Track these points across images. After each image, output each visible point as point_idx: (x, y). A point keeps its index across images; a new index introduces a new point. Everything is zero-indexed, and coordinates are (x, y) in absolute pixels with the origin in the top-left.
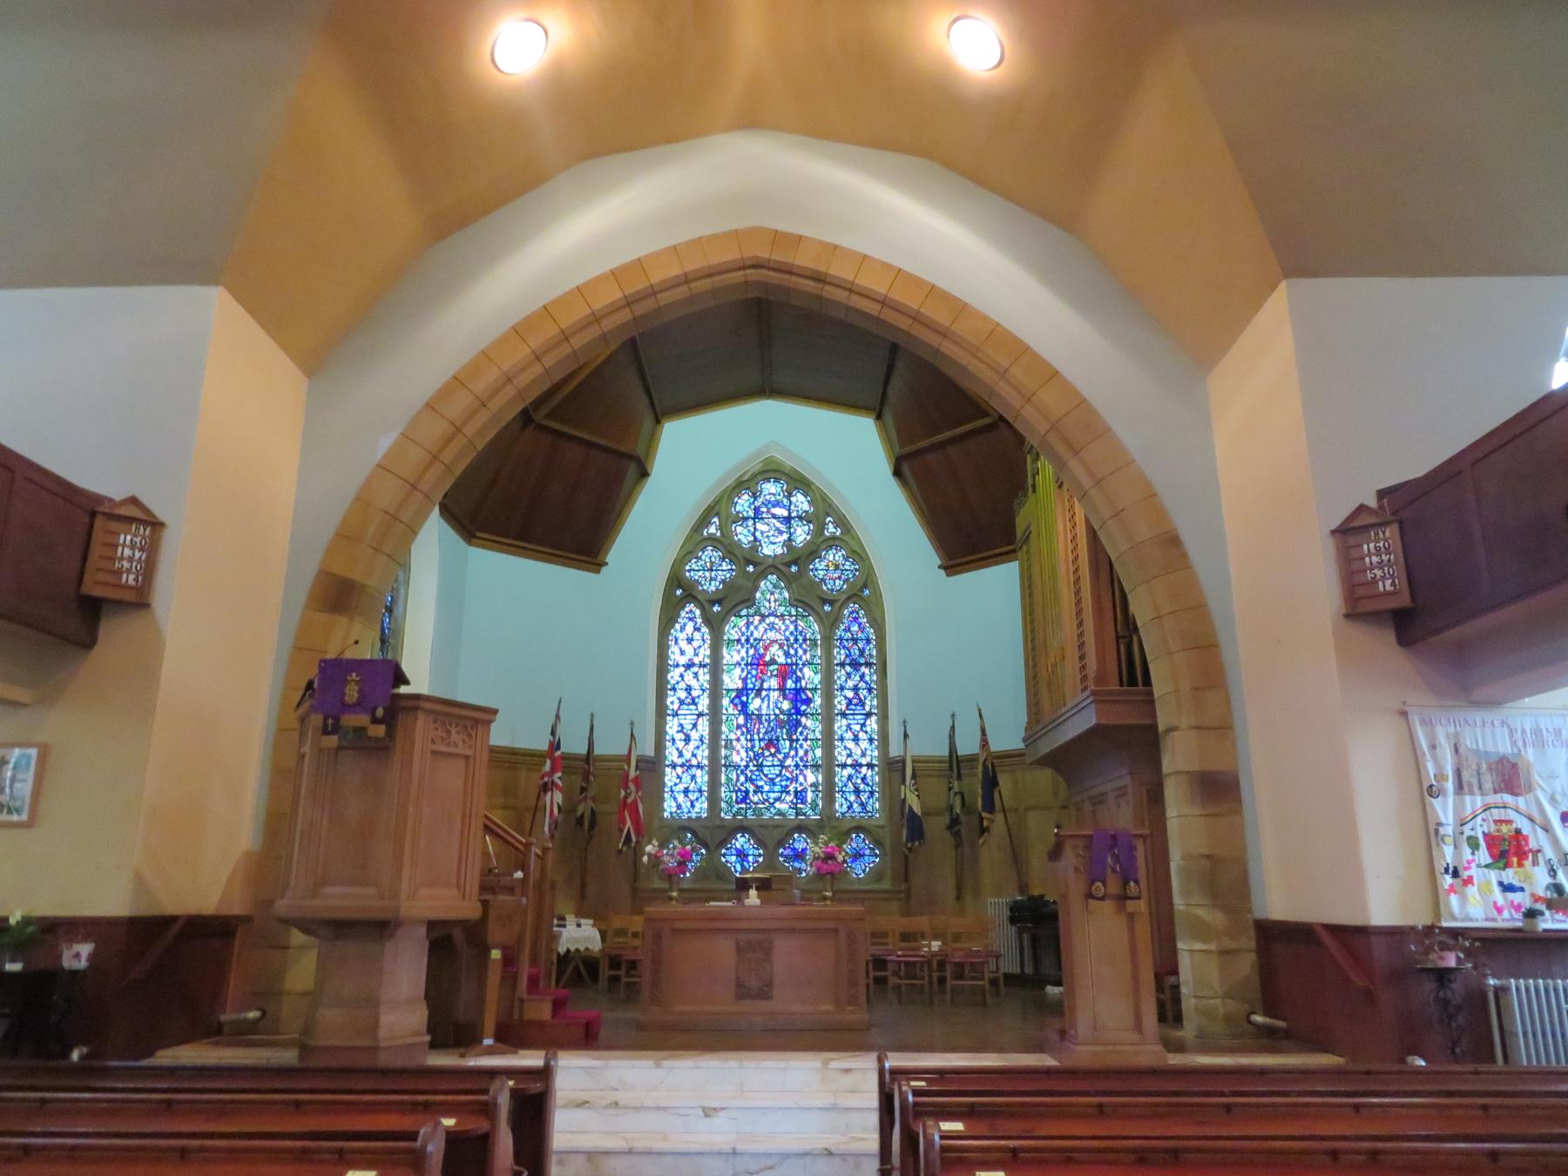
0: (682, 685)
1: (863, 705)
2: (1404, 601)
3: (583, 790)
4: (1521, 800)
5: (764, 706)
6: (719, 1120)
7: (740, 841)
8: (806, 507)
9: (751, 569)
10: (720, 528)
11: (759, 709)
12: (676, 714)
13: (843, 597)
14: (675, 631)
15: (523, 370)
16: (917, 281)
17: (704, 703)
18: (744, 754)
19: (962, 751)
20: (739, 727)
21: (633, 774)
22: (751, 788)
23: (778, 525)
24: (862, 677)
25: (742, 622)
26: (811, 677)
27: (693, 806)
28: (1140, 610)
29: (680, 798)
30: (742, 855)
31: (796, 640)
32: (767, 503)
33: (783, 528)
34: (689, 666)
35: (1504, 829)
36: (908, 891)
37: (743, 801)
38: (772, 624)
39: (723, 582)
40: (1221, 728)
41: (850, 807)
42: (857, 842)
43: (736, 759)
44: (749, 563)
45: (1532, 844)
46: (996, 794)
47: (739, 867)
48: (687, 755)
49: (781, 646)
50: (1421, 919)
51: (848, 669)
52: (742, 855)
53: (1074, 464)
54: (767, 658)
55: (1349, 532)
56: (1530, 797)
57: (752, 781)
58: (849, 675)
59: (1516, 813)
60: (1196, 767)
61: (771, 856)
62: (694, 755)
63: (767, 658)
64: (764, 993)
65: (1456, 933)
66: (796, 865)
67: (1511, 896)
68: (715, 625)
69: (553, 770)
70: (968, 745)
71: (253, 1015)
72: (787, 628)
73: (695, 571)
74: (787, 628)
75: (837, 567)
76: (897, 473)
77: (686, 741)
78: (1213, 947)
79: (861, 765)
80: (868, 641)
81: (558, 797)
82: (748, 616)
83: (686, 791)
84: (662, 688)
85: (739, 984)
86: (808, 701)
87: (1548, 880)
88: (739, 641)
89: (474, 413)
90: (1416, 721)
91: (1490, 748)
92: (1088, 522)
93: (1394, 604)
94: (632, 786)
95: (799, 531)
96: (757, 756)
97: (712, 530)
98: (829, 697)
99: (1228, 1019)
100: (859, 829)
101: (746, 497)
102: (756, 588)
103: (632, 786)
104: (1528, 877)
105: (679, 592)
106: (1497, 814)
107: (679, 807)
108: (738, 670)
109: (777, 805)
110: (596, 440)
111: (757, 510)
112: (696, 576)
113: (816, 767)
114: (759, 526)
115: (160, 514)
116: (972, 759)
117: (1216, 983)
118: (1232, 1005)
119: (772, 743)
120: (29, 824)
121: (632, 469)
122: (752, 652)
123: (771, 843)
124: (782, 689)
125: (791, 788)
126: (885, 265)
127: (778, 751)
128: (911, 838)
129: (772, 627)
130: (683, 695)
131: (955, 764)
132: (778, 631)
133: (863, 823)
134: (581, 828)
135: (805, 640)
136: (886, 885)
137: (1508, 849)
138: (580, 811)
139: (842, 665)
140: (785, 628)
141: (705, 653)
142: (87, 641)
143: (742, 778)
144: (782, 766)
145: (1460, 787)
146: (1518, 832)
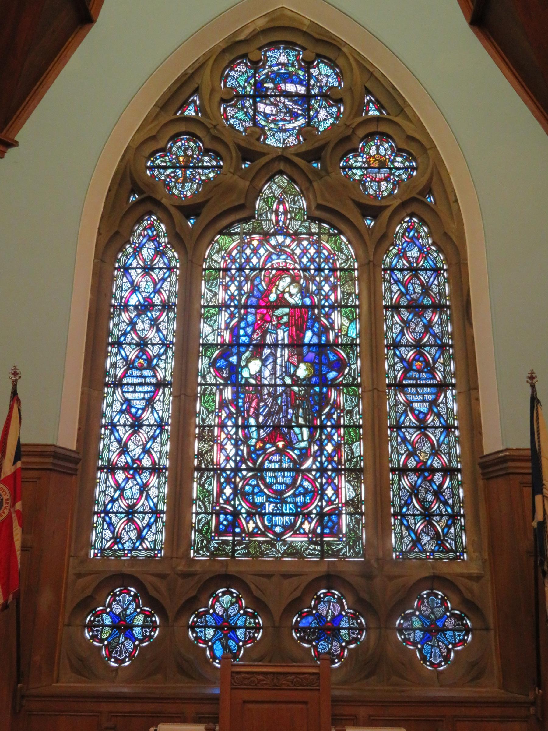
0: (132, 337)
1: (432, 371)
5: (267, 373)
7: (224, 602)
8: (333, 81)
10: (200, 109)
11: (258, 376)
12: (118, 384)
13: (396, 203)
14: (126, 256)
17: (166, 369)
18: (230, 448)
20: (223, 404)
22: (244, 508)
23: (289, 104)
24: (428, 327)
25: (231, 243)
26: (345, 326)
27: (141, 538)
29: (119, 522)
30: (226, 627)
32: (273, 77)
33: (298, 109)
34: (145, 307)
37: (230, 529)
38: (283, 250)
39: (203, 183)
41: (417, 541)
42: (429, 605)
43: (219, 457)
44: (251, 157)
47: (219, 651)
48: (135, 451)
49: (295, 280)
51: (405, 314)
52: (226, 627)
54: (273, 297)
57: (245, 495)
58: (406, 324)
61: (277, 629)
62: (147, 451)
63: (273, 297)
66: (323, 646)
68: (189, 246)
72: (305, 251)
74: (305, 251)
77: (134, 435)
79: (433, 471)
84: (98, 341)
88: (227, 270)
95: (323, 114)
97: (190, 112)
98: (375, 360)
100: (436, 580)
101: (242, 68)
107: (117, 539)
108: (224, 316)
109: (289, 538)
110: (303, 664)
111: (258, 85)
112: (162, 176)
113: (354, 473)
114: (261, 107)
119: (278, 432)
122: (246, 288)
123: (277, 609)
124: (296, 344)
125: (313, 508)
127: (290, 445)
129: (280, 249)
130: (131, 353)
132: (291, 255)
133: (445, 570)
135: (333, 270)
136: (490, 689)
139: (395, 308)
140: (303, 252)
141: (170, 288)
143: (228, 491)
144: (297, 470)
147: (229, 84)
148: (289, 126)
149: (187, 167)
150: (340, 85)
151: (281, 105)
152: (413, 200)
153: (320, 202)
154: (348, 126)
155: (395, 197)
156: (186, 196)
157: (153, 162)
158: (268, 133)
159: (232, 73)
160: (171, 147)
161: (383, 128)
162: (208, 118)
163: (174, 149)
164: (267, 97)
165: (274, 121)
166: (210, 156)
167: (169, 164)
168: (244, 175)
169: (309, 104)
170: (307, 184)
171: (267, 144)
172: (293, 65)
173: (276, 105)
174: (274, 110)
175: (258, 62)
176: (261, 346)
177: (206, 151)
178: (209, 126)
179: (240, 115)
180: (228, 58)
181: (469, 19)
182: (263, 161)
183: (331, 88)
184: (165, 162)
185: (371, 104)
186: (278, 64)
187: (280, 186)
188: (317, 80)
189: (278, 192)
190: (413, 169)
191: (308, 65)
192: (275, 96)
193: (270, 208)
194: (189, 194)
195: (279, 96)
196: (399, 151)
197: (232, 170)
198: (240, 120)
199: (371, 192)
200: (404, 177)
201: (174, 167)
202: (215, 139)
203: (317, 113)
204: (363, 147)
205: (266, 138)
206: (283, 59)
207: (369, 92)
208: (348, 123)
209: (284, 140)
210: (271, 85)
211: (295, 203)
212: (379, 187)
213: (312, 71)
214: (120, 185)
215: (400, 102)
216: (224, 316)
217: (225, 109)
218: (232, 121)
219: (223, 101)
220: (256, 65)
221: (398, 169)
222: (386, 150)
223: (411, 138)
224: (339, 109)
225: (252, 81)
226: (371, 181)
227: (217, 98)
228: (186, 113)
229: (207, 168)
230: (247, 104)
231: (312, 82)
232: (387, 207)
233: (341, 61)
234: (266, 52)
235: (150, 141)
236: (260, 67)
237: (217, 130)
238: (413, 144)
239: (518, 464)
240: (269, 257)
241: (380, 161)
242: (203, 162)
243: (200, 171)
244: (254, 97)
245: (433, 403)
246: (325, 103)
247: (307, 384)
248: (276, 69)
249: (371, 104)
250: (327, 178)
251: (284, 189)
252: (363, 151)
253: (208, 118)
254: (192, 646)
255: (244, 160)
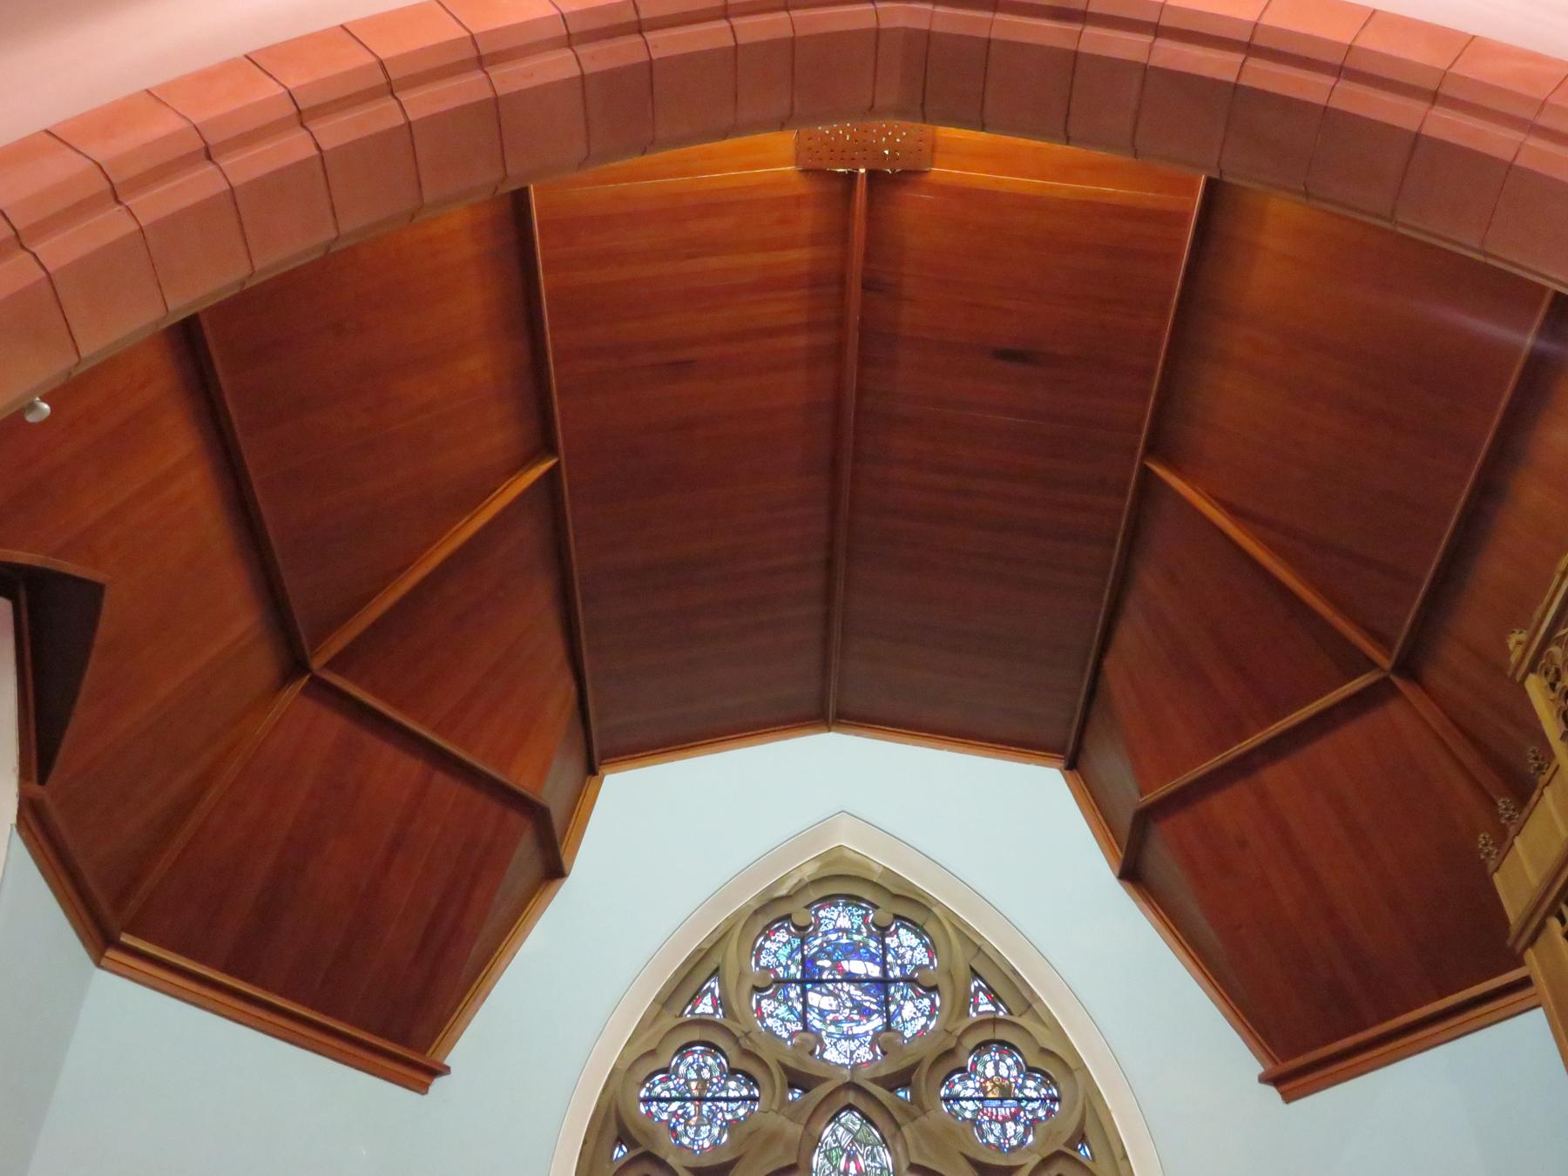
8: (921, 956)
10: (721, 1002)
13: (1033, 1161)
15: (246, 139)
33: (870, 1002)
39: (730, 1126)
76: (1131, 873)
89: (80, 209)
95: (909, 1010)
97: (705, 1007)
101: (782, 936)
105: (619, 1153)
112: (663, 1113)
114: (814, 998)
121: (525, 851)
147: (763, 962)
148: (857, 1030)
149: (702, 1099)
150: (931, 962)
151: (844, 996)
152: (1058, 1155)
153: (916, 1160)
154: (949, 1033)
155: (1030, 1149)
156: (702, 1149)
157: (649, 1090)
158: (827, 1041)
159: (768, 944)
160: (677, 1065)
161: (1003, 1034)
162: (736, 1020)
163: (682, 1069)
164: (821, 982)
165: (835, 1022)
166: (738, 1080)
167: (674, 1093)
168: (793, 1111)
169: (887, 993)
170: (893, 1129)
171: (825, 1061)
172: (859, 932)
173: (837, 997)
174: (835, 1003)
175: (806, 928)
177: (733, 1072)
178: (738, 1034)
179: (782, 1011)
180: (764, 921)
181: (1117, 870)
182: (820, 1092)
183: (919, 968)
184: (669, 1090)
185: (981, 994)
186: (836, 930)
187: (849, 1130)
188: (897, 956)
189: (846, 1140)
190: (1054, 1100)
191: (882, 932)
192: (834, 981)
193: (835, 1168)
194: (707, 1144)
195: (841, 981)
196: (1030, 1071)
197: (775, 1107)
198: (783, 1020)
199: (992, 1139)
200: (1041, 1113)
201: (683, 1099)
202: (748, 1060)
203: (901, 1007)
204: (974, 1063)
205: (823, 1050)
206: (844, 922)
207: (976, 975)
208: (950, 1028)
209: (852, 1053)
210: (826, 963)
211: (874, 1160)
212: (1004, 1130)
213: (888, 940)
214: (601, 1133)
215: (1026, 994)
217: (758, 1002)
218: (770, 1022)
219: (757, 989)
220: (803, 932)
221: (1030, 1100)
222: (1009, 1068)
223: (1045, 1051)
224: (933, 1001)
225: (799, 957)
226: (990, 1121)
227: (747, 987)
228: (698, 1011)
229: (735, 1100)
230: (793, 994)
231: (890, 958)
232: (1018, 1168)
233: (931, 927)
234: (817, 910)
235: (644, 1060)
236: (809, 935)
237: (751, 1040)
238: (1050, 1060)
241: (1001, 1087)
242: (727, 1090)
243: (723, 1105)
244: (802, 982)
246: (911, 993)
248: (833, 937)
249: (981, 994)
250: (924, 1119)
251: (855, 1135)
252: (974, 1070)
253: (736, 1020)
255: (792, 1086)
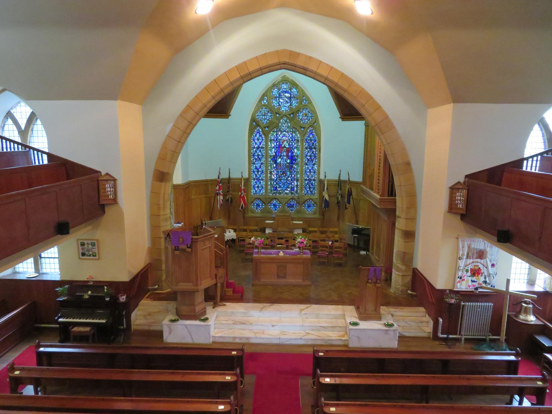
2: (464, 213)
3: (228, 191)
4: (482, 261)
6: (276, 328)
7: (274, 202)
8: (296, 93)
9: (278, 115)
11: (280, 162)
16: (336, 71)
19: (342, 178)
20: (274, 168)
21: (243, 188)
24: (313, 152)
28: (396, 183)
30: (275, 206)
31: (292, 140)
32: (283, 92)
35: (476, 268)
36: (324, 219)
40: (412, 219)
41: (307, 192)
43: (273, 177)
45: (482, 271)
46: (351, 197)
49: (287, 142)
50: (449, 287)
52: (275, 206)
53: (382, 137)
55: (453, 189)
56: (485, 260)
59: (480, 264)
60: (404, 229)
64: (284, 277)
65: (458, 292)
67: (473, 283)
69: (219, 189)
70: (344, 177)
71: (156, 287)
73: (259, 117)
75: (306, 115)
78: (401, 274)
80: (315, 141)
81: (222, 197)
82: (277, 131)
83: (258, 187)
85: (278, 275)
86: (296, 160)
87: (484, 280)
88: (274, 140)
89: (203, 108)
90: (460, 240)
91: (478, 248)
92: (385, 152)
93: (462, 212)
94: (242, 191)
96: (279, 177)
99: (402, 291)
102: (280, 122)
103: (242, 191)
104: (479, 279)
106: (475, 264)
107: (256, 191)
111: (279, 94)
115: (116, 177)
116: (345, 182)
117: (400, 283)
118: (403, 288)
120: (98, 259)
124: (287, 156)
126: (327, 65)
127: (286, 175)
128: (325, 207)
129: (284, 135)
131: (340, 183)
132: (286, 137)
134: (228, 203)
136: (317, 216)
137: (476, 272)
138: (227, 197)
139: (306, 148)
142: (104, 212)
145: (468, 257)
146: (479, 268)
176: (281, 156)
202: (271, 109)
206: (285, 87)
216: (273, 150)
239: (255, 74)
240: (282, 137)
245: (312, 168)
247: (289, 163)
254: (270, 208)
